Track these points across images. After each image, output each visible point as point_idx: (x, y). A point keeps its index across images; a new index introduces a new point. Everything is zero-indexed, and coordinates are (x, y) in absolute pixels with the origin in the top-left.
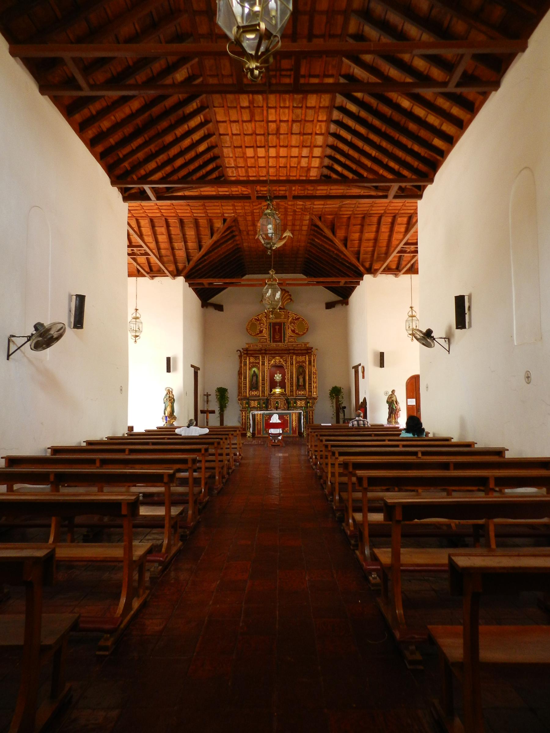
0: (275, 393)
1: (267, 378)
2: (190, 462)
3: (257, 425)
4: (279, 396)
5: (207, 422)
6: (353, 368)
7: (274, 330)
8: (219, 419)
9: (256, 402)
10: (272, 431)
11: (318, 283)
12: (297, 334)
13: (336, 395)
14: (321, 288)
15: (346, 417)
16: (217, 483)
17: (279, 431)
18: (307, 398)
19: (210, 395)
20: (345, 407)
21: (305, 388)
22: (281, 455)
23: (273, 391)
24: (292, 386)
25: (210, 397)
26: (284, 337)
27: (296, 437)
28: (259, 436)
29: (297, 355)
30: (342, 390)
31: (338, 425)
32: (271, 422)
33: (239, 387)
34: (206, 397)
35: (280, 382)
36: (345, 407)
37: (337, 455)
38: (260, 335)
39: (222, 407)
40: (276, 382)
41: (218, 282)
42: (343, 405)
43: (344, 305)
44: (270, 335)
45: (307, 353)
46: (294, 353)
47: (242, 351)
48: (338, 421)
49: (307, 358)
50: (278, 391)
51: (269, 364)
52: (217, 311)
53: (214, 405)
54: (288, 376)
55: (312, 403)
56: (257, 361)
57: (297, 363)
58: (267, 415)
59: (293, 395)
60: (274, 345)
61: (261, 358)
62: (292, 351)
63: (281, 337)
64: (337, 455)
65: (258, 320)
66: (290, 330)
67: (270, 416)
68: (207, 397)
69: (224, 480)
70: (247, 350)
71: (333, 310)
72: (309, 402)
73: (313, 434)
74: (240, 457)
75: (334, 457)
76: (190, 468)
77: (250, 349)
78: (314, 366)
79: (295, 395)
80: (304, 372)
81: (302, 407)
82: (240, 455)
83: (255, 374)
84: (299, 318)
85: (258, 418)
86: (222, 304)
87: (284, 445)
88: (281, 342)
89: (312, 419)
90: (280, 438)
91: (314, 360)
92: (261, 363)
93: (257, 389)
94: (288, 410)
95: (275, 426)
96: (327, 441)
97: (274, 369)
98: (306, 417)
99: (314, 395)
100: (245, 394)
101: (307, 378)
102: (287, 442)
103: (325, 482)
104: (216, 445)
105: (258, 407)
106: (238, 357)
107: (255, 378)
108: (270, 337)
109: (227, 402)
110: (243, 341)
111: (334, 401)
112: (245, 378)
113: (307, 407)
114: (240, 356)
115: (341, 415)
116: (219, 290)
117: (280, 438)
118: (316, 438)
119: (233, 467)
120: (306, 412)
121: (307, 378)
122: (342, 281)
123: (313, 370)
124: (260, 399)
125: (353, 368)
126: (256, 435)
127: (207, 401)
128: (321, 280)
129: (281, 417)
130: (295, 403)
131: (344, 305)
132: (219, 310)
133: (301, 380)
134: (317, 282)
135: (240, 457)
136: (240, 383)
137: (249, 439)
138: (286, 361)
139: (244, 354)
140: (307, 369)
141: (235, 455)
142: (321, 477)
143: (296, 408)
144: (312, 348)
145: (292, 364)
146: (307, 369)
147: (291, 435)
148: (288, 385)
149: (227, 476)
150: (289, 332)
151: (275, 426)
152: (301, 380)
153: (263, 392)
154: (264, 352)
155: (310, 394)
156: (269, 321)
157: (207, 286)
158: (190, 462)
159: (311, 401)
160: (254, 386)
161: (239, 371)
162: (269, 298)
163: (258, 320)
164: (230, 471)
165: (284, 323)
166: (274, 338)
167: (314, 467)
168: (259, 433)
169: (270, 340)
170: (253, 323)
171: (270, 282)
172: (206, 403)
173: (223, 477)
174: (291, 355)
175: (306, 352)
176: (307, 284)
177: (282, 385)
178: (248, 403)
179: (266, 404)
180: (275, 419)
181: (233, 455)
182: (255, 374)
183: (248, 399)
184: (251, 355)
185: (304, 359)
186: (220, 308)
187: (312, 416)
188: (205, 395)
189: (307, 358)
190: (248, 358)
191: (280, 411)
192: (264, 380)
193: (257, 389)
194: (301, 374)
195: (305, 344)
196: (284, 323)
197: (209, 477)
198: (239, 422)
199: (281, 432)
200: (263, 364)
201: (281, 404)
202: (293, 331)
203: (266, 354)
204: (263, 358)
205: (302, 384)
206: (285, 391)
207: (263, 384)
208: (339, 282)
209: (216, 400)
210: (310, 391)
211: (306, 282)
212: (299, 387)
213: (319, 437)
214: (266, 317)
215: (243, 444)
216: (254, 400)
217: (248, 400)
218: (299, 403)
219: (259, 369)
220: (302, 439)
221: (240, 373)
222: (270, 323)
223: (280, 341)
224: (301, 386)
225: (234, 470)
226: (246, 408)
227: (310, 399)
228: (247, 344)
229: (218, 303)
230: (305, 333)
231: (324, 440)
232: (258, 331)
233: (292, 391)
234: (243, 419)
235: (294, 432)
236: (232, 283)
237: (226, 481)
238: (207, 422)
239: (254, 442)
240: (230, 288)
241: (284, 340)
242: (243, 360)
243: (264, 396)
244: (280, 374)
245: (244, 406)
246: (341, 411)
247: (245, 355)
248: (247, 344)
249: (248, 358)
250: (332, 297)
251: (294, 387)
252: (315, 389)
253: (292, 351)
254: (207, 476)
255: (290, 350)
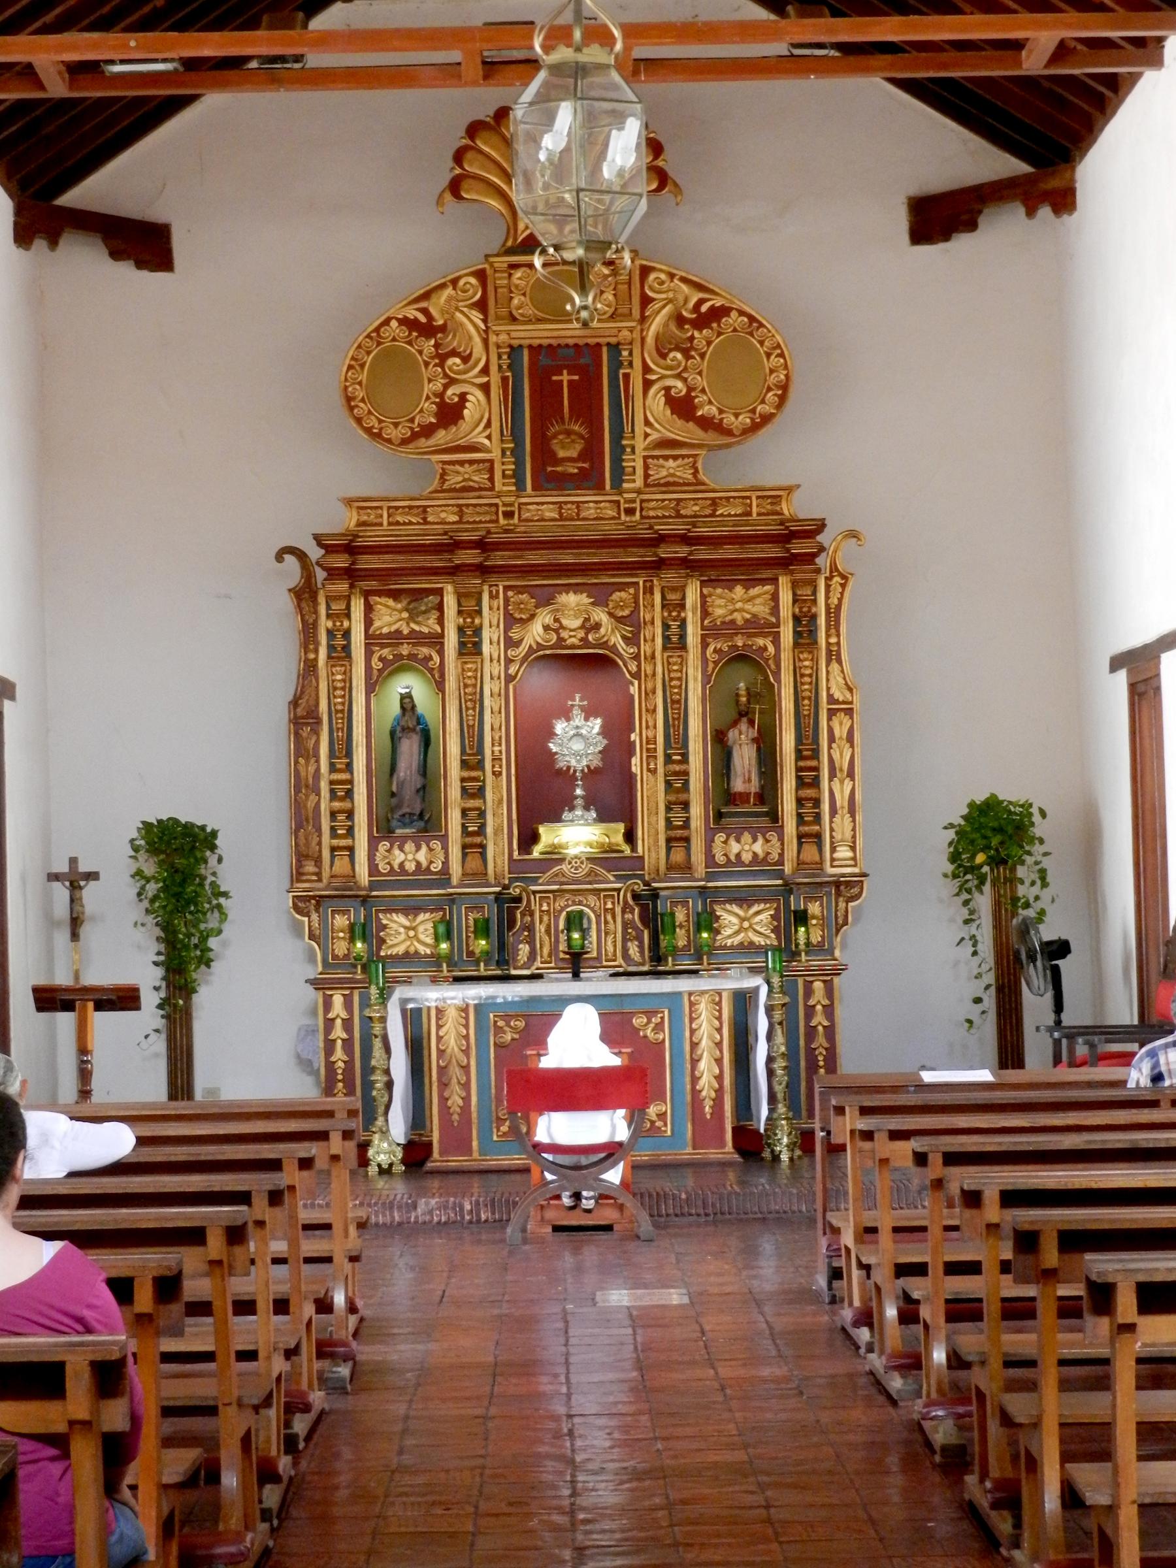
0: (554, 857)
1: (497, 742)
2: (79, 1385)
3: (444, 1085)
4: (592, 877)
5: (85, 1075)
6: (1117, 663)
7: (545, 394)
8: (159, 1045)
9: (425, 924)
10: (560, 1128)
11: (856, 54)
12: (706, 423)
13: (997, 861)
14: (874, 93)
15: (1068, 1019)
16: (233, 1520)
17: (604, 1126)
18: (788, 888)
19: (92, 876)
20: (1061, 949)
21: (774, 817)
22: (619, 1297)
23: (548, 835)
24: (678, 802)
25: (90, 892)
26: (618, 450)
27: (724, 1165)
28: (456, 1161)
29: (717, 573)
30: (1040, 828)
31: (1012, 1075)
32: (546, 1063)
33: (302, 820)
34: (61, 892)
35: (591, 774)
36: (1061, 949)
37: (1126, 1303)
38: (441, 437)
39: (182, 963)
40: (567, 776)
41: (136, 58)
42: (1048, 932)
43: (1045, 212)
44: (517, 435)
45: (787, 563)
46: (689, 565)
47: (315, 553)
48: (1010, 1054)
49: (786, 597)
50: (577, 835)
51: (511, 643)
52: (126, 271)
53: (124, 950)
54: (650, 729)
55: (824, 921)
56: (429, 625)
57: (709, 633)
58: (509, 1012)
59: (686, 868)
60: (542, 510)
61: (450, 601)
62: (682, 551)
63: (592, 452)
64: (1126, 1303)
65: (427, 329)
66: (657, 403)
67: (538, 1022)
68: (74, 887)
69: (272, 1496)
70: (350, 546)
71: (962, 244)
72: (802, 918)
73: (883, 1147)
74: (353, 1320)
75: (1104, 1323)
76: (86, 1424)
77: (372, 537)
78: (834, 655)
79: (700, 869)
80: (765, 694)
81: (749, 948)
82: (352, 1308)
83: (411, 724)
84: (718, 313)
85: (449, 1037)
86: (157, 214)
87: (645, 1225)
88: (599, 487)
89: (830, 1032)
90: (614, 1176)
91: (834, 615)
92: (451, 640)
93: (427, 823)
94: (655, 974)
95: (577, 1090)
96: (1011, 1198)
97: (543, 683)
98: (787, 1019)
99: (839, 861)
100: (341, 865)
101: (787, 742)
102: (661, 1204)
103: (1010, 1498)
104: (215, 1244)
105: (436, 960)
106: (287, 603)
107: (410, 748)
108: (517, 453)
109: (212, 921)
110: (328, 481)
111: (984, 902)
112: (343, 750)
113: (788, 951)
114: (305, 594)
115: (1035, 1006)
116: (141, 114)
117: (614, 1176)
118: (919, 1178)
119: (317, 1398)
120: (788, 988)
121: (787, 742)
122: (1041, 39)
123: (833, 683)
124: (452, 899)
125: (1117, 663)
126: (437, 1159)
127: (75, 923)
128: (888, 29)
129: (616, 1026)
130: (707, 921)
131: (1045, 212)
132: (140, 265)
133: (744, 757)
134: (842, 47)
135: (353, 1320)
136: (302, 787)
137: (381, 1183)
138: (633, 625)
139: (333, 574)
140: (787, 678)
141: (324, 1306)
142: (956, 1461)
143: (703, 958)
144: (821, 526)
145: (675, 644)
146: (787, 678)
147: (687, 1152)
148: (651, 792)
149: (284, 1464)
150: (650, 415)
151: (577, 1090)
152: (744, 757)
153: (474, 846)
154: (478, 558)
155: (810, 853)
156: (503, 334)
157: (57, 88)
158: (79, 1385)
159: (814, 908)
160: (409, 810)
161: (295, 703)
162: (560, 165)
163: (427, 329)
164: (300, 1425)
165: (615, 348)
166: (544, 454)
167: (896, 1383)
168: (458, 1140)
169: (518, 478)
170: (388, 355)
171: (563, 54)
172: (62, 936)
173: (267, 1474)
174: (670, 576)
175: (773, 551)
176: (792, 65)
177: (613, 797)
178: (366, 931)
179: (497, 934)
180: (577, 1042)
181: (309, 1310)
182: (411, 724)
183: (365, 900)
184: (385, 584)
185: (760, 608)
186: (143, 244)
187: (829, 1011)
188: (54, 877)
189: (786, 597)
190: (357, 607)
191: (597, 983)
192: (480, 765)
193: (427, 823)
194: (744, 714)
195: (774, 497)
196: (615, 348)
197: (190, 1482)
198: (305, 1064)
199: (623, 1134)
200: (470, 646)
201: (607, 935)
202: (682, 407)
203: (483, 571)
204: (470, 610)
205: (754, 787)
206: (630, 837)
207: (473, 791)
208: (1017, 46)
209: (136, 912)
210: (810, 837)
211: (779, 48)
212: (726, 807)
213: (936, 1168)
214: (482, 306)
215: (362, 1225)
216: (412, 909)
217: (366, 904)
218: (729, 918)
219: (440, 685)
220: (762, 1181)
221: (303, 717)
222: (515, 351)
223: (589, 479)
224: (743, 798)
225: (322, 1413)
226: (359, 972)
227: (817, 888)
228: (349, 502)
229: (130, 206)
230: (766, 419)
231: (991, 1196)
232: (427, 412)
233: (678, 838)
234: (329, 1046)
235: (706, 1131)
236: (235, 63)
237: (284, 1504)
238: (85, 1075)
239: (429, 1206)
240: (214, 105)
241: (619, 474)
242: (324, 624)
243: (480, 876)
244: (589, 714)
245: (341, 948)
246: (1034, 978)
247: (342, 586)
248: (349, 502)
249: (357, 607)
250: (959, 156)
251: (696, 811)
252: (843, 824)
253: (682, 551)
254: (171, 1476)
255: (661, 539)
